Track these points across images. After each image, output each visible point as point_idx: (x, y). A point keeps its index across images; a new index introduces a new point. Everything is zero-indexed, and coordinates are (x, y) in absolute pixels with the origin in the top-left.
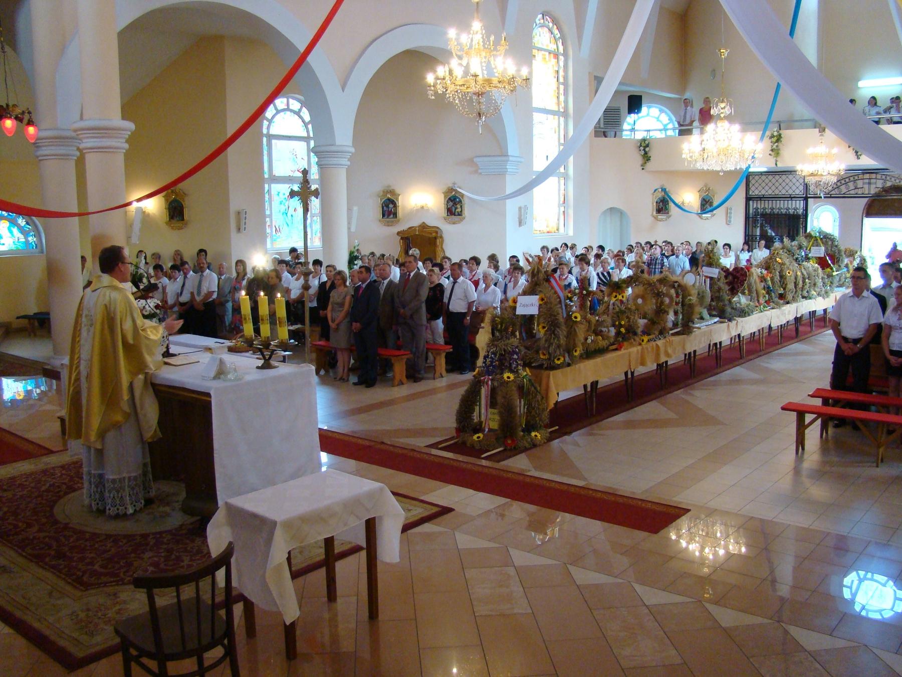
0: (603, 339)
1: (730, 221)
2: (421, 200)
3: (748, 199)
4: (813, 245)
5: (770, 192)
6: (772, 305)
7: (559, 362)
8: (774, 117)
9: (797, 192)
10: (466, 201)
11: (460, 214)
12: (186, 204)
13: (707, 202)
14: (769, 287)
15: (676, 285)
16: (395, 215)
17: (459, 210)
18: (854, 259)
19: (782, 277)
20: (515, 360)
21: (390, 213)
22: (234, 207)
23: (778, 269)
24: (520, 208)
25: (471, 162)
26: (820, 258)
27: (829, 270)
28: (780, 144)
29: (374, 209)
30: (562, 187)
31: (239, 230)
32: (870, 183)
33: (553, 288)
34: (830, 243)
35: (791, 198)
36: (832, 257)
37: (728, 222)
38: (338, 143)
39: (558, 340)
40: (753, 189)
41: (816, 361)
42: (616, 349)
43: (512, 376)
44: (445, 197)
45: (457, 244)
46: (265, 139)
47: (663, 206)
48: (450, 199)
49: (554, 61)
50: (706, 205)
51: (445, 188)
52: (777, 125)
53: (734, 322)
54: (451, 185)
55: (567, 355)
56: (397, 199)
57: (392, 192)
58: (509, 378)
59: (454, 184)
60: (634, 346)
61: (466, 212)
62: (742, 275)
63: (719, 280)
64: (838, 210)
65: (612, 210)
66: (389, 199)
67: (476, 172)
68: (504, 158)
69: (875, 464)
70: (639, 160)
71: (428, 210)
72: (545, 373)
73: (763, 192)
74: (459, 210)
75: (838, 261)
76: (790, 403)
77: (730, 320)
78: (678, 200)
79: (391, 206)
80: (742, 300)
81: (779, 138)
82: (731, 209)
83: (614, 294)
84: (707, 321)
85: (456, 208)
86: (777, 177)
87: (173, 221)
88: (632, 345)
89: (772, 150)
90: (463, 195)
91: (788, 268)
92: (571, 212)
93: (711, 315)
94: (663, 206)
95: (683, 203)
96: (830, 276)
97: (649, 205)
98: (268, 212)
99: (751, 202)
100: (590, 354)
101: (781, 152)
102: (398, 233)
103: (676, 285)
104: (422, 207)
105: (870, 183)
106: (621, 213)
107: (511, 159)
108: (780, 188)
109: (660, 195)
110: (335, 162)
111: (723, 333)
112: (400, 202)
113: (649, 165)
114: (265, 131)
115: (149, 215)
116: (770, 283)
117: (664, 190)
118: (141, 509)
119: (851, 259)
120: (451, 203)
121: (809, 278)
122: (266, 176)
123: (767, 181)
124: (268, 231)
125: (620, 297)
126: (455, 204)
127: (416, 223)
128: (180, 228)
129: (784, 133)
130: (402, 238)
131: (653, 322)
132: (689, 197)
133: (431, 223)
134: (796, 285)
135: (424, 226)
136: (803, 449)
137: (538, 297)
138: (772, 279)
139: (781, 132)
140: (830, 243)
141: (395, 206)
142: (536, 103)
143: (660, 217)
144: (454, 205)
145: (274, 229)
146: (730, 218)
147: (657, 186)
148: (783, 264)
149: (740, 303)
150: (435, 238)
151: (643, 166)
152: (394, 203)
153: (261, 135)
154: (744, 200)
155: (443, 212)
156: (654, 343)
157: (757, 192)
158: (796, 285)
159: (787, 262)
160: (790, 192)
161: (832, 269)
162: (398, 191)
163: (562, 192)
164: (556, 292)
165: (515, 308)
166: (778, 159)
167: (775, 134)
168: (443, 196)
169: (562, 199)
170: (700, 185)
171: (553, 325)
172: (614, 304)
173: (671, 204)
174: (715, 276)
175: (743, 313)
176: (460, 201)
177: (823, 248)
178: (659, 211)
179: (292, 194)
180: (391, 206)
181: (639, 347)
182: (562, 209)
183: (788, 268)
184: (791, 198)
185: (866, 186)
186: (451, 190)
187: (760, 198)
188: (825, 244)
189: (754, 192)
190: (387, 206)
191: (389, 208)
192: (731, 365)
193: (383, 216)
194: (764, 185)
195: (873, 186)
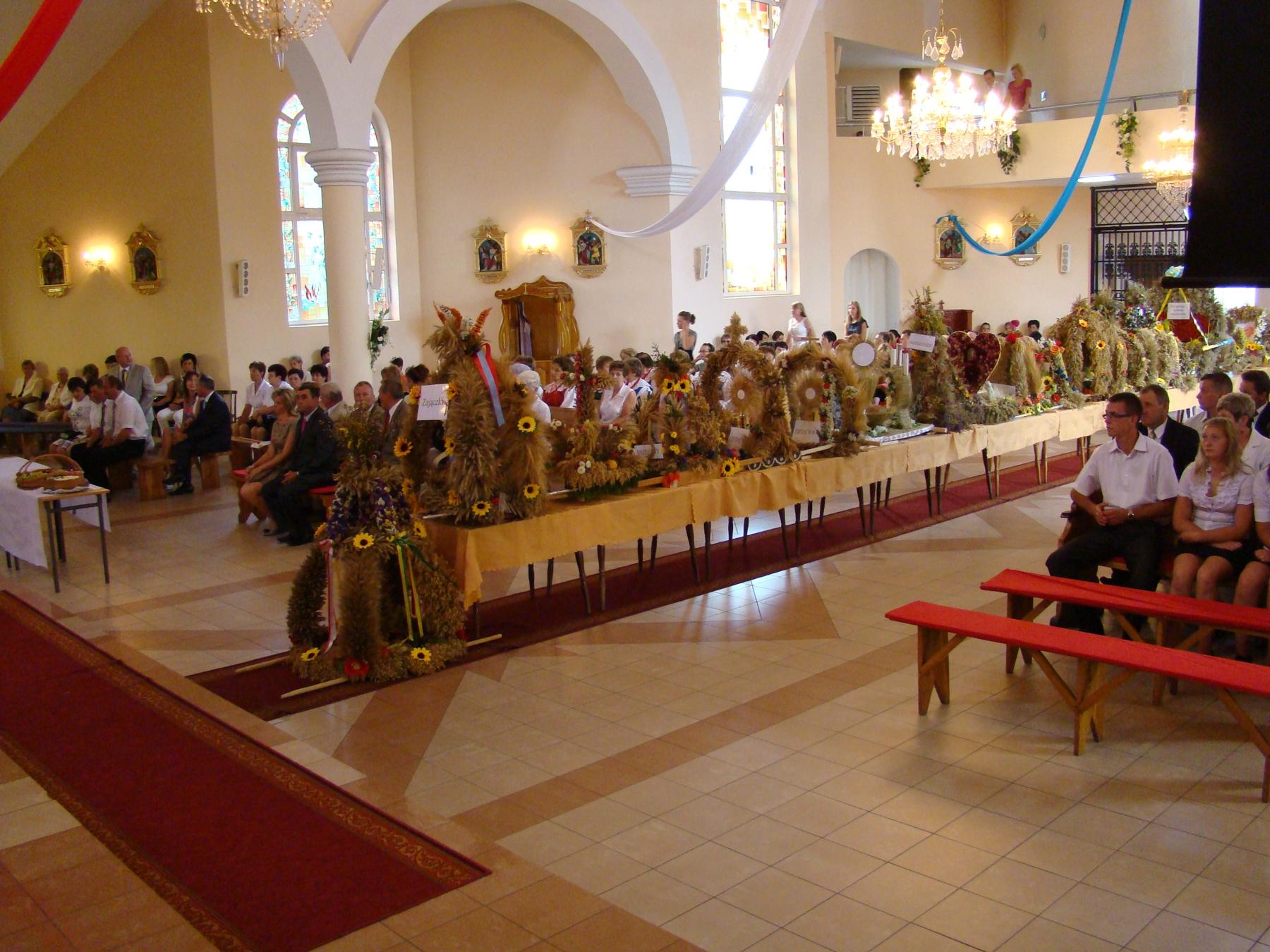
0: (620, 465)
1: (1065, 268)
2: (539, 241)
3: (1096, 231)
4: (1170, 300)
5: (1131, 218)
6: (1064, 401)
7: (483, 513)
8: (1121, 88)
10: (606, 241)
11: (598, 262)
12: (159, 253)
14: (1059, 371)
15: (826, 364)
16: (499, 265)
17: (597, 255)
18: (1257, 325)
19: (1087, 352)
20: (381, 509)
21: (491, 263)
22: (227, 256)
23: (1081, 339)
24: (698, 251)
25: (612, 177)
26: (1183, 322)
27: (1196, 341)
28: (1133, 135)
30: (781, 217)
31: (237, 292)
33: (478, 368)
35: (1165, 227)
36: (1203, 320)
37: (1063, 270)
38: (341, 145)
39: (476, 469)
40: (1103, 214)
41: (1050, 510)
42: (660, 485)
43: (370, 540)
44: (575, 234)
46: (283, 153)
47: (953, 244)
48: (582, 238)
49: (761, 14)
50: (1025, 241)
51: (572, 220)
52: (1130, 104)
53: (966, 434)
54: (583, 216)
55: (503, 497)
56: (502, 240)
57: (494, 230)
58: (364, 542)
60: (704, 478)
61: (607, 258)
62: (990, 348)
63: (937, 356)
65: (870, 252)
66: (489, 241)
67: (622, 193)
68: (665, 170)
69: (1072, 749)
71: (549, 256)
72: (460, 531)
73: (1120, 219)
74: (597, 255)
75: (1213, 327)
76: (919, 604)
77: (957, 429)
78: (976, 235)
79: (493, 251)
80: (993, 392)
81: (1131, 126)
82: (1066, 247)
83: (666, 381)
84: (908, 430)
85: (592, 252)
86: (1131, 194)
87: (142, 281)
88: (699, 478)
89: (1121, 146)
90: (602, 232)
91: (1099, 337)
92: (796, 256)
93: (921, 421)
94: (953, 244)
95: (985, 239)
96: (1197, 352)
97: (929, 243)
98: (289, 264)
99: (1100, 236)
100: (578, 496)
101: (1135, 148)
102: (497, 294)
103: (826, 364)
104: (540, 252)
106: (887, 260)
107: (674, 170)
109: (947, 227)
110: (335, 177)
111: (960, 451)
112: (506, 246)
114: (282, 136)
115: (108, 272)
116: (1062, 364)
117: (953, 219)
118: (359, 681)
119: (1251, 324)
120: (584, 245)
121: (1148, 355)
122: (286, 206)
123: (1125, 200)
124: (290, 292)
125: (677, 387)
126: (590, 245)
127: (532, 278)
128: (152, 292)
129: (1143, 116)
130: (505, 302)
131: (757, 434)
132: (995, 230)
133: (555, 276)
134: (1115, 364)
135: (543, 282)
136: (944, 700)
138: (1067, 357)
139: (1135, 114)
142: (726, 83)
143: (949, 262)
144: (588, 247)
145: (304, 292)
146: (1065, 262)
147: (943, 212)
148: (1087, 330)
149: (987, 398)
150: (555, 301)
151: (918, 181)
152: (496, 246)
153: (275, 145)
154: (1089, 233)
155: (572, 259)
156: (756, 474)
157: (1109, 220)
158: (1115, 364)
159: (1098, 326)
160: (1164, 218)
161: (1202, 340)
162: (501, 229)
163: (781, 225)
164: (482, 377)
165: (415, 408)
166: (1131, 160)
167: (1125, 117)
168: (570, 233)
169: (781, 236)
170: (1015, 209)
171: (470, 438)
172: (666, 399)
173: (966, 245)
174: (930, 350)
175: (990, 416)
176: (598, 241)
177: (1188, 305)
178: (946, 253)
180: (493, 251)
181: (717, 483)
182: (783, 252)
183: (1099, 337)
184: (1165, 227)
186: (584, 223)
187: (1116, 229)
189: (1105, 219)
190: (487, 252)
191: (490, 255)
192: (962, 511)
194: (1120, 207)
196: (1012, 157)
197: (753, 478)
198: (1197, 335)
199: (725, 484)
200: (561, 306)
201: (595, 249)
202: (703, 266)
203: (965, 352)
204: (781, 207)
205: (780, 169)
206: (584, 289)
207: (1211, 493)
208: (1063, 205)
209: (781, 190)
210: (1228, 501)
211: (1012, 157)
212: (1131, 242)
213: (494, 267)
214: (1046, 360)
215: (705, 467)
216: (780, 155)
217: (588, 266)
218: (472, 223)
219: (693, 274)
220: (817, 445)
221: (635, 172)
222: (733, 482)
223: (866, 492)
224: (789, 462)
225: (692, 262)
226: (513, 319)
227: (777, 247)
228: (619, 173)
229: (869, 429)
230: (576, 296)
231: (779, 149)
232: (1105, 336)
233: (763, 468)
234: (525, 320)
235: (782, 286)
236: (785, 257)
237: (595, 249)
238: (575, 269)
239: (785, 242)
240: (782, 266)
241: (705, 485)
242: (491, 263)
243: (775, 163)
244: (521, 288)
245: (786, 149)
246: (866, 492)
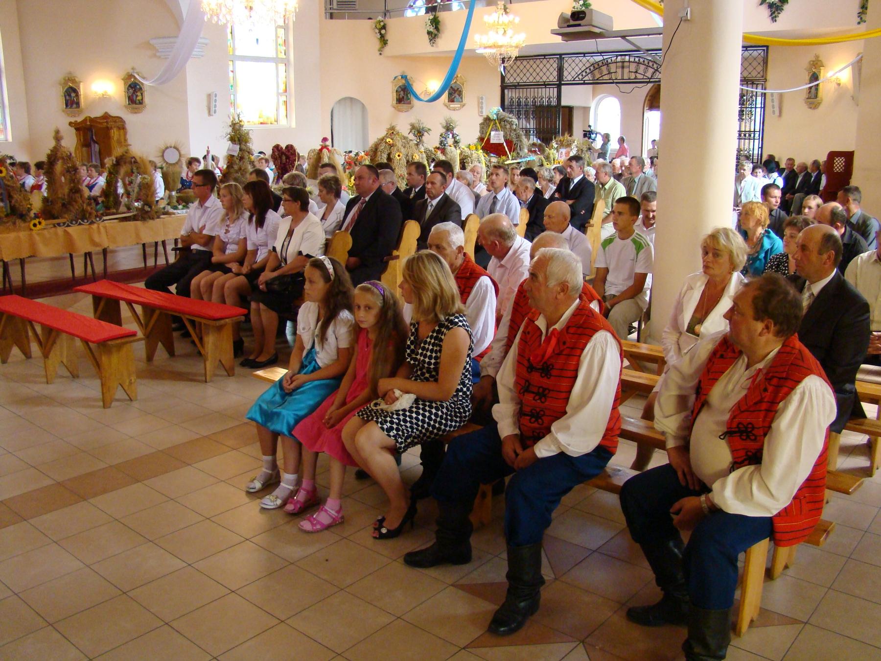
2: (102, 88)
3: (504, 87)
9: (551, 78)
10: (145, 88)
11: (141, 102)
13: (455, 91)
16: (78, 104)
17: (139, 98)
21: (73, 103)
25: (148, 45)
27: (504, 158)
29: (56, 99)
32: (623, 67)
34: (508, 126)
44: (125, 84)
45: (143, 139)
47: (404, 95)
48: (130, 86)
51: (123, 74)
54: (131, 71)
59: (133, 69)
61: (147, 100)
64: (615, 97)
66: (71, 88)
67: (155, 56)
70: (377, 44)
73: (518, 80)
74: (139, 98)
79: (73, 95)
82: (482, 98)
85: (137, 96)
88: (9, 231)
91: (398, 150)
92: (293, 100)
94: (404, 95)
97: (390, 96)
99: (506, 91)
105: (623, 67)
108: (541, 74)
112: (82, 92)
113: (387, 50)
117: (404, 77)
119: (568, 149)
126: (135, 92)
127: (97, 113)
130: (77, 129)
133: (114, 113)
137: (72, 150)
140: (508, 126)
141: (77, 95)
143: (402, 106)
144: (134, 92)
148: (391, 146)
155: (124, 101)
157: (512, 80)
163: (282, 79)
168: (123, 82)
169: (282, 88)
176: (141, 89)
177: (502, 133)
178: (400, 100)
179: (648, 223)
180: (73, 95)
181: (27, 233)
183: (398, 150)
184: (545, 85)
185: (619, 71)
186: (130, 76)
187: (516, 86)
188: (503, 128)
190: (70, 95)
191: (71, 97)
193: (67, 105)
195: (626, 70)
196: (436, 35)
197: (56, 234)
198: (505, 154)
199: (31, 237)
200: (115, 134)
201: (139, 94)
202: (213, 109)
203: (280, 157)
204: (282, 67)
205: (281, 41)
206: (131, 120)
207: (227, 231)
208: (457, 65)
209: (282, 56)
210: (235, 236)
211: (436, 35)
212: (532, 95)
213: (75, 106)
214: (356, 165)
215: (14, 223)
216: (281, 32)
217: (134, 106)
218: (59, 75)
219: (206, 112)
220: (124, 213)
221: (161, 41)
222: (38, 234)
223: (150, 251)
224: (92, 223)
225: (205, 103)
226: (85, 140)
227: (279, 94)
228: (152, 42)
229: (176, 204)
230: (128, 126)
231: (281, 27)
232: (403, 150)
233: (68, 226)
234: (95, 142)
235: (283, 121)
236: (286, 102)
237: (139, 94)
238: (126, 107)
239: (286, 91)
240: (282, 108)
241: (13, 235)
242: (73, 103)
243: (277, 37)
244: (85, 120)
245: (286, 28)
246: (150, 251)
